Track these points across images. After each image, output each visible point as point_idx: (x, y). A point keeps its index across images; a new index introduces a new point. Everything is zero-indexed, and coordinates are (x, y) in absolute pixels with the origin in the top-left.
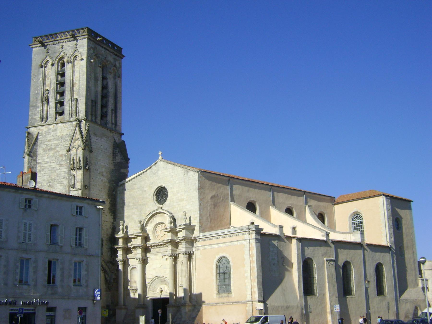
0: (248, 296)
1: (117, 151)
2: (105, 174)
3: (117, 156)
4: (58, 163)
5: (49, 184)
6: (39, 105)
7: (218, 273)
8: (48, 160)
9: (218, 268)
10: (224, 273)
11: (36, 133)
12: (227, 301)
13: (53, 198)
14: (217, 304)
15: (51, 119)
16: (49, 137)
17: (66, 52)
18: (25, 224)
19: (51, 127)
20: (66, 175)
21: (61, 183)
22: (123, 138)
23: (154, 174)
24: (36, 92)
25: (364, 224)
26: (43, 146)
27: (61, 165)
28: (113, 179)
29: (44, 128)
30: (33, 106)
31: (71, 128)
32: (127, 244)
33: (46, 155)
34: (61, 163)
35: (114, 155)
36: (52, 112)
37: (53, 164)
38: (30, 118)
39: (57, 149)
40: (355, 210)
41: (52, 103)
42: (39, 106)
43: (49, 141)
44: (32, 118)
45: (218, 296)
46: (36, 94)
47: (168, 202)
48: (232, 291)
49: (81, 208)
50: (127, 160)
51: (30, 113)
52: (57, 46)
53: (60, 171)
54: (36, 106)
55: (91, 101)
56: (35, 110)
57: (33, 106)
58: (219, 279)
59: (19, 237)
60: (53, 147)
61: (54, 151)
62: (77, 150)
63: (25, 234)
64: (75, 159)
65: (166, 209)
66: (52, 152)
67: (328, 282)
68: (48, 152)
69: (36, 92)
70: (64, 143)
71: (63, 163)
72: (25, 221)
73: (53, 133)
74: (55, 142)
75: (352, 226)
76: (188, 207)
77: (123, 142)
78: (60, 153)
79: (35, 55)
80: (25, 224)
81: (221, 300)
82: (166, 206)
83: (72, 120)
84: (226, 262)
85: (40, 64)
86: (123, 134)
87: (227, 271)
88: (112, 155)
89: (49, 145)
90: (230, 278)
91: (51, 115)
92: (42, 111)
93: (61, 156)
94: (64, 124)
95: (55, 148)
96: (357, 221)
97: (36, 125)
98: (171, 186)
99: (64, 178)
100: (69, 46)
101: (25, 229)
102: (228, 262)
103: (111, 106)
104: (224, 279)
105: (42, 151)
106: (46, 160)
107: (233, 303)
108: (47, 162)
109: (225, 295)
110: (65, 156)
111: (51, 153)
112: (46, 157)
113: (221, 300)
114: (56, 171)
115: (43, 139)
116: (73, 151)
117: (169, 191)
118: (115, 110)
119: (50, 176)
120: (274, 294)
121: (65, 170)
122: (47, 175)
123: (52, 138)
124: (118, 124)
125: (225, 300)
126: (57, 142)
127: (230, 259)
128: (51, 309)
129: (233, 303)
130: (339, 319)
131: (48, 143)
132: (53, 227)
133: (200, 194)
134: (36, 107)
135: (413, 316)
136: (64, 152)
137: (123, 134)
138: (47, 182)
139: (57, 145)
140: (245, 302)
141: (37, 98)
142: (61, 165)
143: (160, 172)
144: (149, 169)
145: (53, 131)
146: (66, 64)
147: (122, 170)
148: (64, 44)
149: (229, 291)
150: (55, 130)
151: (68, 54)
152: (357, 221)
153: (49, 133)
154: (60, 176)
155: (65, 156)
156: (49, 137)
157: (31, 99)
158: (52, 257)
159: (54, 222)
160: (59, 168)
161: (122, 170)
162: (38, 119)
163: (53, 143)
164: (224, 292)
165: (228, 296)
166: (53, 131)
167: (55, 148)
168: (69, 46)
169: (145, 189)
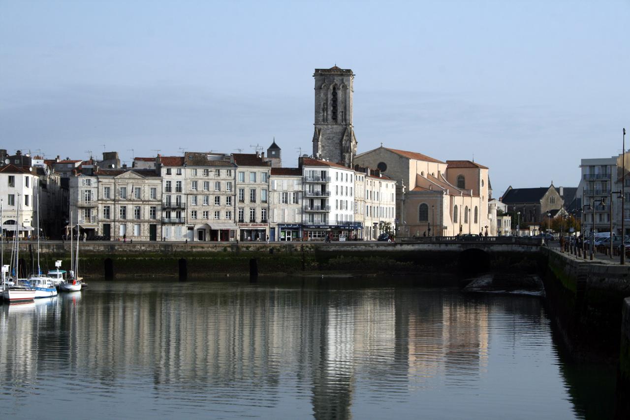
14: (419, 226)
20: (340, 155)
21: (337, 158)
27: (336, 149)
32: (596, 228)
54: (319, 112)
60: (331, 138)
67: (530, 290)
71: (337, 147)
81: (421, 224)
91: (208, 232)
95: (332, 139)
113: (421, 224)
120: (288, 167)
125: (424, 224)
133: (316, 94)
135: (8, 348)
139: (334, 137)
142: (336, 149)
153: (328, 129)
167: (332, 139)
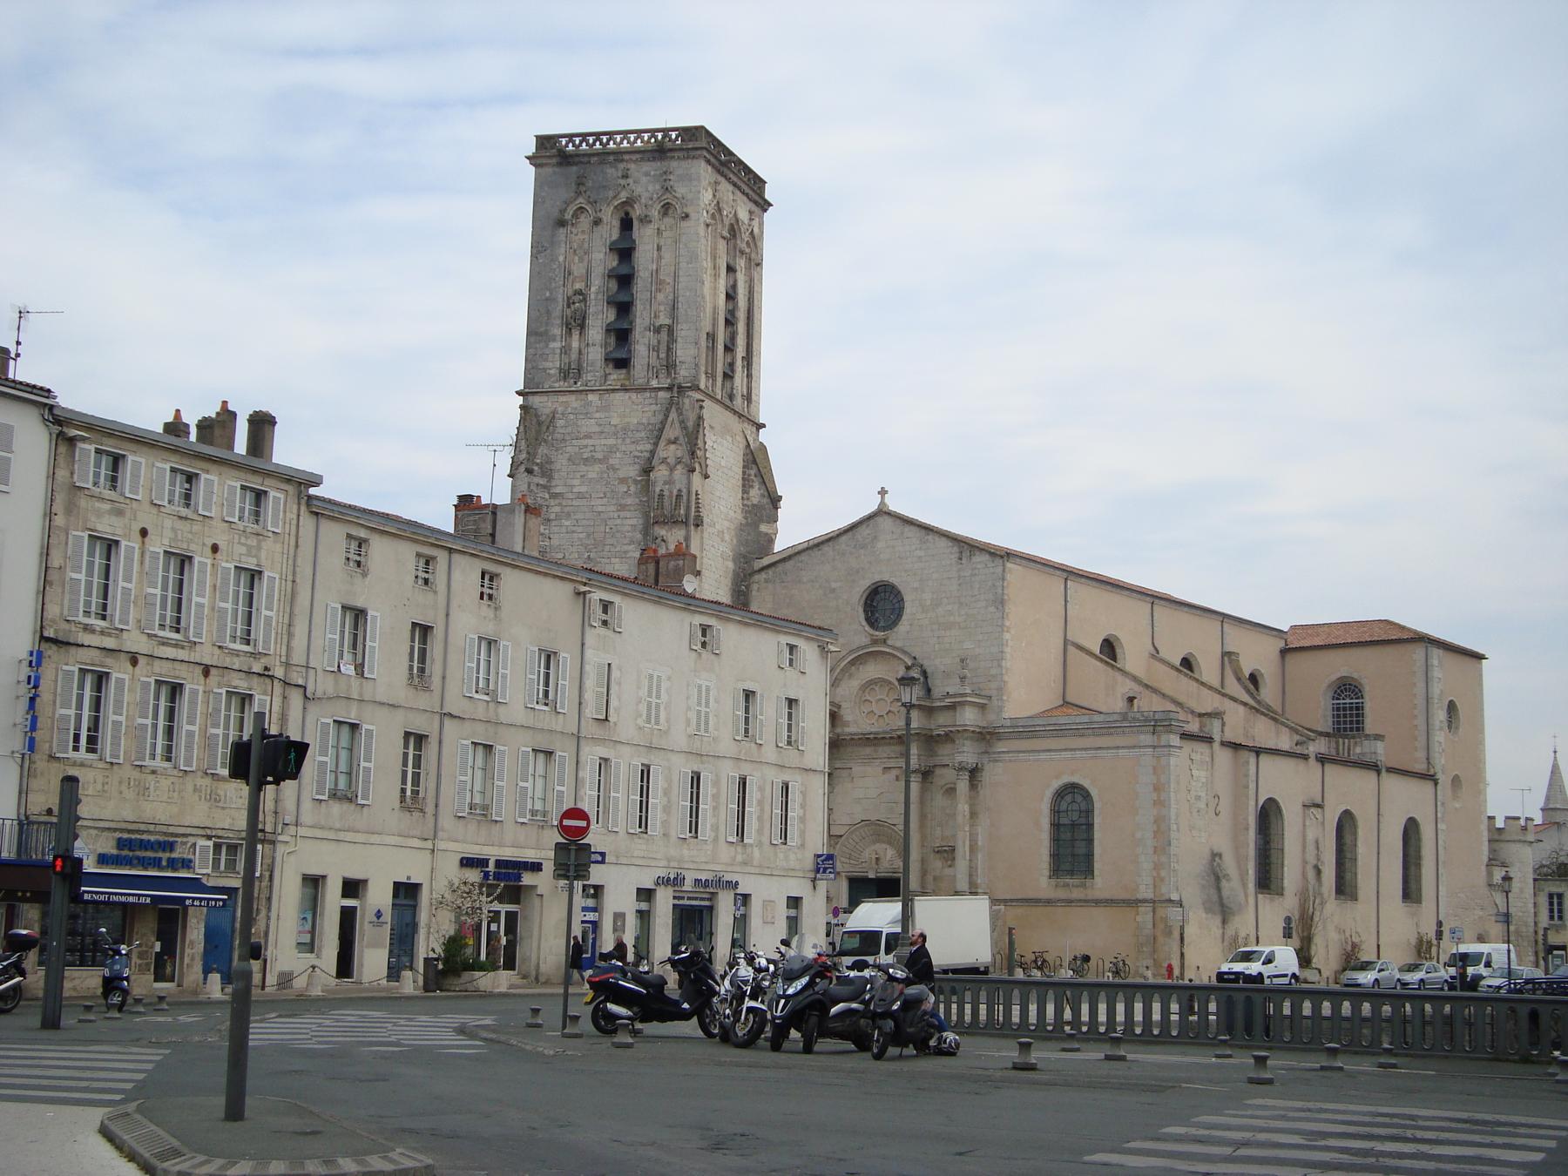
0: (1142, 888)
1: (752, 472)
2: (727, 537)
6: (557, 331)
7: (1056, 826)
8: (583, 489)
9: (1056, 811)
10: (1073, 825)
12: (1082, 896)
13: (746, 624)
14: (1049, 902)
15: (591, 376)
16: (588, 426)
17: (639, 190)
18: (700, 686)
22: (764, 436)
23: (863, 547)
25: (1367, 711)
26: (569, 449)
31: (654, 407)
35: (746, 485)
36: (596, 355)
37: (599, 502)
39: (611, 461)
40: (1344, 672)
41: (596, 332)
43: (588, 436)
45: (1053, 881)
47: (903, 627)
48: (1096, 872)
50: (775, 501)
52: (610, 171)
58: (1056, 840)
59: (688, 722)
60: (599, 456)
62: (672, 470)
64: (666, 493)
65: (898, 644)
66: (597, 467)
70: (633, 447)
71: (629, 501)
75: (1330, 713)
76: (968, 645)
77: (763, 448)
78: (621, 474)
82: (900, 635)
83: (654, 383)
84: (1079, 799)
85: (555, 214)
86: (764, 426)
87: (1083, 821)
88: (740, 483)
90: (1090, 841)
92: (566, 350)
93: (623, 481)
94: (634, 395)
97: (546, 388)
98: (916, 585)
99: (631, 542)
100: (647, 174)
101: (699, 704)
102: (1087, 796)
103: (740, 351)
104: (1073, 840)
105: (565, 462)
107: (1097, 902)
108: (580, 496)
109: (1076, 882)
110: (636, 482)
111: (593, 472)
112: (576, 482)
113: (1062, 894)
116: (660, 473)
117: (908, 598)
118: (749, 359)
121: (634, 522)
123: (597, 429)
124: (754, 397)
125: (1076, 894)
126: (611, 441)
127: (1094, 793)
129: (1097, 902)
130: (675, 882)
131: (585, 442)
136: (632, 471)
137: (764, 426)
138: (582, 549)
139: (612, 450)
140: (1134, 903)
141: (548, 312)
142: (622, 507)
143: (880, 545)
146: (635, 223)
147: (764, 528)
148: (632, 166)
149: (1089, 871)
150: (606, 408)
151: (645, 196)
155: (636, 482)
156: (588, 426)
159: (750, 686)
161: (764, 528)
163: (602, 443)
164: (1071, 873)
165: (1084, 886)
169: (834, 585)
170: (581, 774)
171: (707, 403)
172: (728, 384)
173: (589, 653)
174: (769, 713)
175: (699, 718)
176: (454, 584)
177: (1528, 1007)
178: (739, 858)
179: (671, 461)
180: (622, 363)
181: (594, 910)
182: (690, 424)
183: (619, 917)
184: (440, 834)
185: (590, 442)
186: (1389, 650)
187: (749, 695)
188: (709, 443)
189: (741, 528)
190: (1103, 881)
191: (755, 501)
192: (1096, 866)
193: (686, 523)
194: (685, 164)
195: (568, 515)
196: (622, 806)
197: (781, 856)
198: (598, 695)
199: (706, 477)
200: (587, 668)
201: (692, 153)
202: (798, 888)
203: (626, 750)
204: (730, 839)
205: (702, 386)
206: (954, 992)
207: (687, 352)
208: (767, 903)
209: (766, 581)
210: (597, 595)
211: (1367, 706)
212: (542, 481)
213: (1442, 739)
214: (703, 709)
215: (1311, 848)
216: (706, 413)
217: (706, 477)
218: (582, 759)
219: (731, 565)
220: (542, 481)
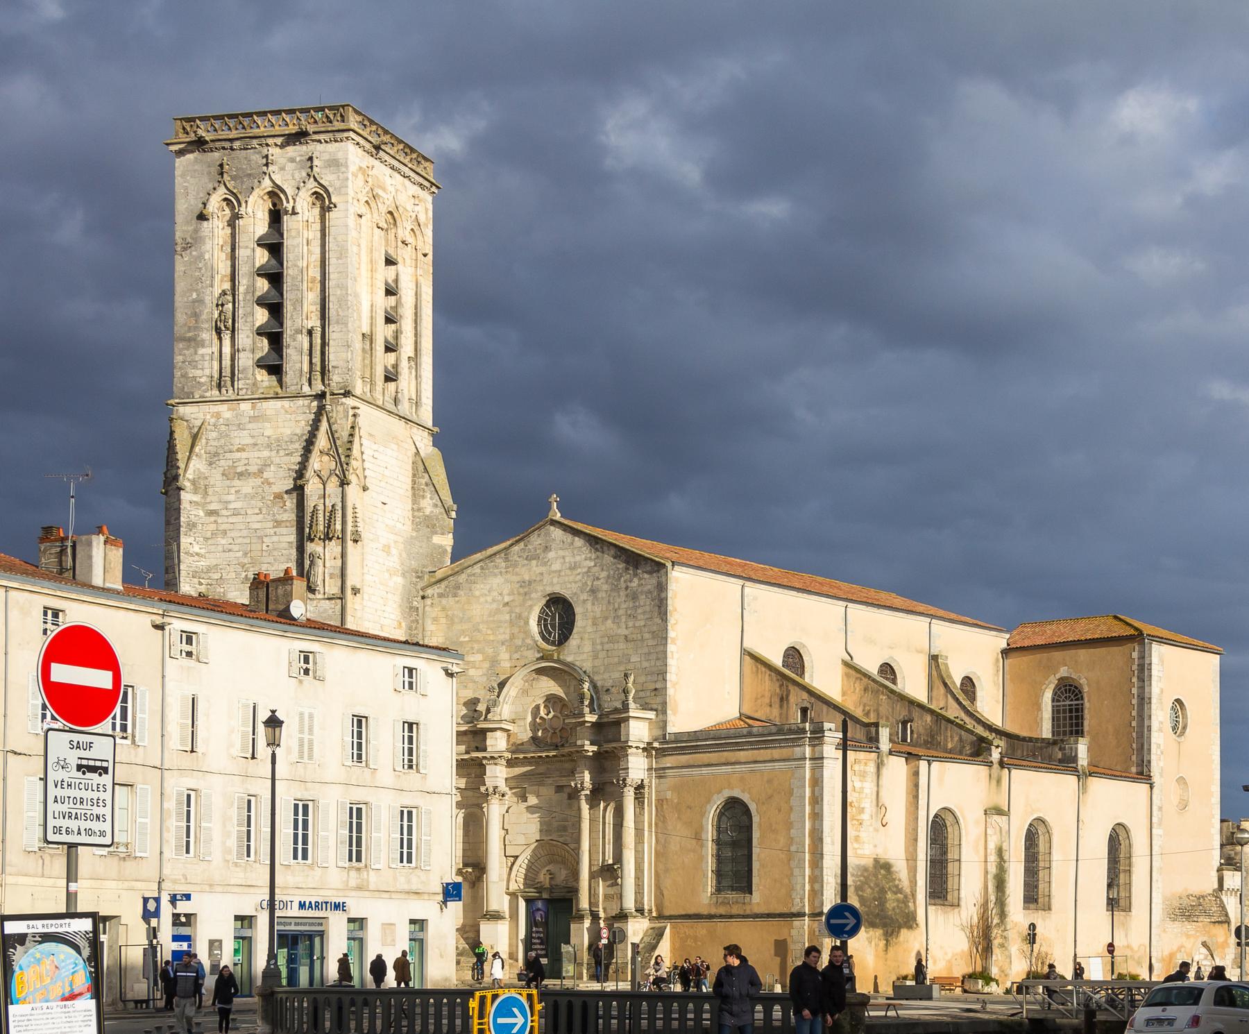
3: (423, 497)
4: (270, 518)
5: (244, 574)
11: (198, 423)
16: (242, 438)
18: (302, 714)
19: (245, 406)
23: (536, 557)
24: (194, 296)
26: (222, 463)
28: (414, 564)
29: (223, 408)
30: (183, 339)
33: (233, 491)
34: (279, 518)
38: (178, 374)
39: (265, 475)
42: (203, 341)
44: (184, 376)
46: (194, 301)
49: (411, 670)
51: (178, 359)
53: (275, 539)
55: (360, 337)
56: (192, 350)
57: (183, 339)
60: (253, 469)
61: (259, 481)
63: (301, 741)
64: (321, 507)
68: (236, 482)
69: (194, 296)
72: (301, 709)
73: (250, 426)
74: (257, 454)
79: (183, 176)
80: (302, 714)
88: (410, 493)
89: (239, 460)
94: (286, 403)
95: (261, 471)
96: (1068, 703)
97: (197, 397)
100: (292, 160)
101: (301, 731)
105: (219, 477)
106: (231, 506)
111: (247, 487)
114: (265, 539)
115: (223, 441)
119: (245, 554)
122: (236, 548)
126: (266, 453)
127: (753, 807)
128: (358, 923)
131: (238, 455)
132: (360, 721)
134: (194, 342)
142: (278, 523)
144: (517, 542)
145: (253, 419)
152: (1068, 703)
153: (240, 427)
154: (275, 553)
156: (242, 438)
157: (181, 317)
158: (359, 795)
160: (272, 532)
162: (202, 380)
166: (253, 419)
167: (261, 471)
168: (292, 160)
170: (166, 805)
171: (364, 410)
172: (392, 385)
173: (170, 685)
174: (385, 742)
175: (301, 745)
176: (11, 624)
177: (566, 999)
178: (353, 883)
179: (325, 474)
180: (275, 370)
181: (187, 938)
182: (343, 434)
183: (214, 944)
184: (8, 869)
185: (244, 455)
186: (166, 720)
187: (360, 721)
188: (368, 453)
189: (410, 542)
190: (758, 899)
191: (428, 511)
192: (755, 880)
193: (343, 540)
194: (333, 147)
195: (225, 532)
196: (217, 836)
197: (402, 879)
198: (183, 726)
199: (365, 489)
200: (169, 700)
201: (339, 136)
202: (428, 909)
203: (216, 781)
204: (340, 864)
205: (358, 392)
206: (366, 1003)
207: (346, 356)
208: (388, 927)
209: (441, 596)
210: (177, 625)
211: (1087, 705)
212: (197, 498)
213: (1161, 741)
214: (306, 737)
215: (993, 858)
216: (361, 421)
217: (365, 489)
218: (167, 791)
219: (399, 580)
220: (197, 498)
